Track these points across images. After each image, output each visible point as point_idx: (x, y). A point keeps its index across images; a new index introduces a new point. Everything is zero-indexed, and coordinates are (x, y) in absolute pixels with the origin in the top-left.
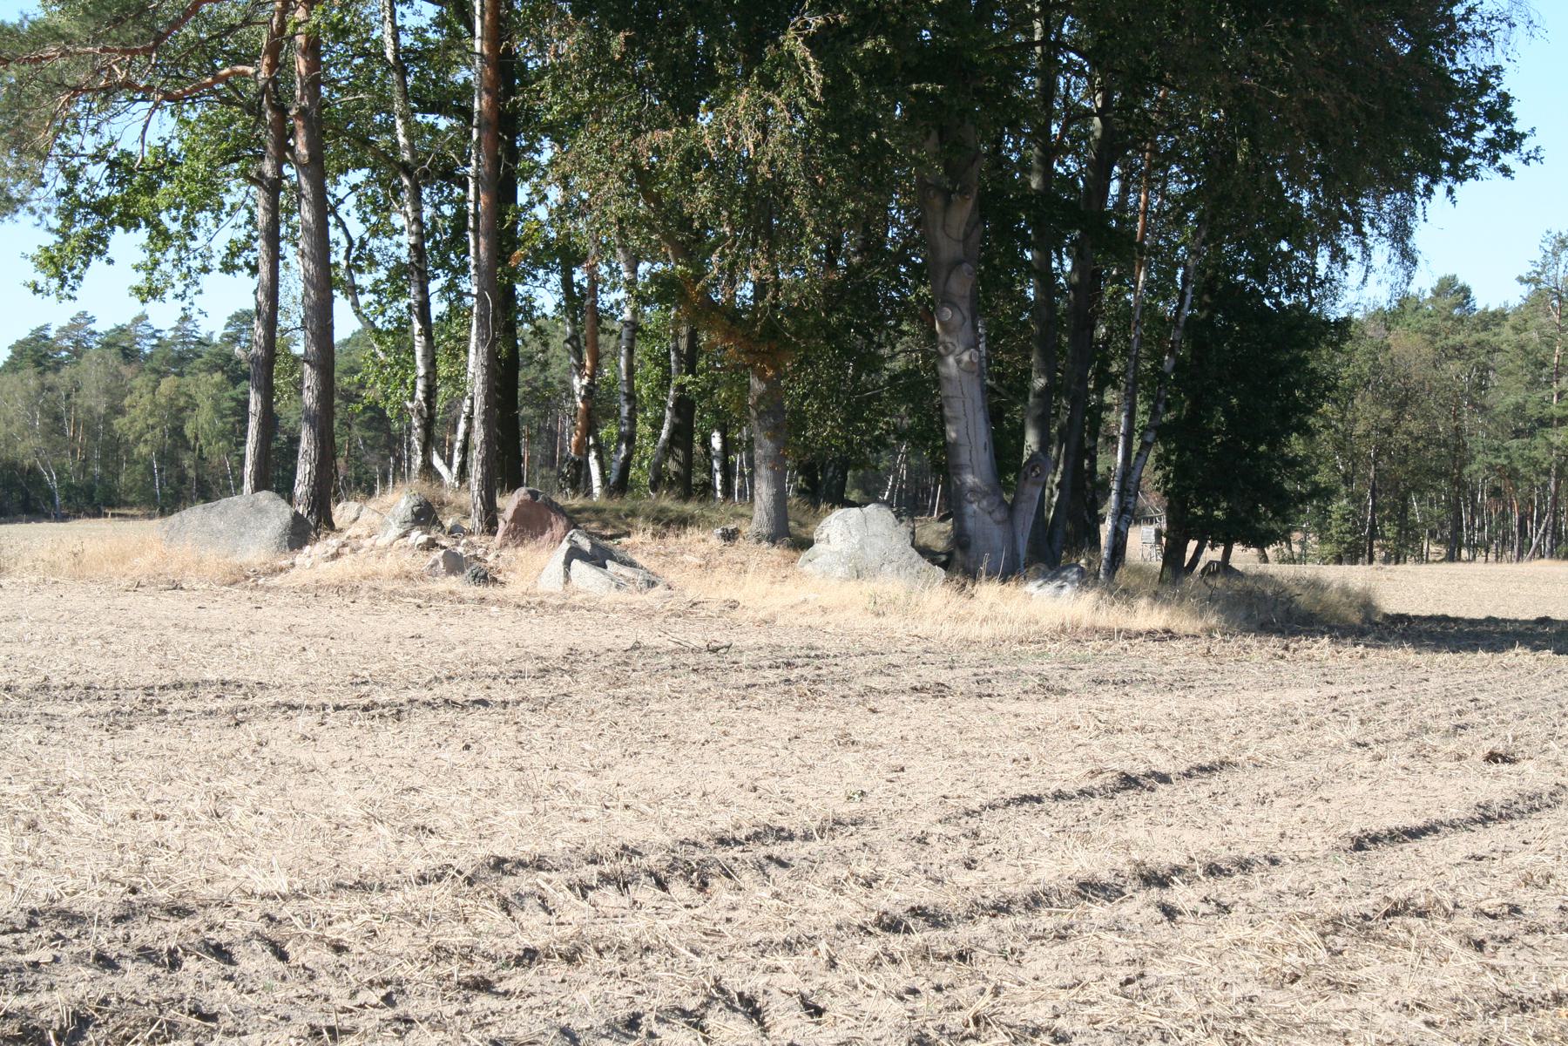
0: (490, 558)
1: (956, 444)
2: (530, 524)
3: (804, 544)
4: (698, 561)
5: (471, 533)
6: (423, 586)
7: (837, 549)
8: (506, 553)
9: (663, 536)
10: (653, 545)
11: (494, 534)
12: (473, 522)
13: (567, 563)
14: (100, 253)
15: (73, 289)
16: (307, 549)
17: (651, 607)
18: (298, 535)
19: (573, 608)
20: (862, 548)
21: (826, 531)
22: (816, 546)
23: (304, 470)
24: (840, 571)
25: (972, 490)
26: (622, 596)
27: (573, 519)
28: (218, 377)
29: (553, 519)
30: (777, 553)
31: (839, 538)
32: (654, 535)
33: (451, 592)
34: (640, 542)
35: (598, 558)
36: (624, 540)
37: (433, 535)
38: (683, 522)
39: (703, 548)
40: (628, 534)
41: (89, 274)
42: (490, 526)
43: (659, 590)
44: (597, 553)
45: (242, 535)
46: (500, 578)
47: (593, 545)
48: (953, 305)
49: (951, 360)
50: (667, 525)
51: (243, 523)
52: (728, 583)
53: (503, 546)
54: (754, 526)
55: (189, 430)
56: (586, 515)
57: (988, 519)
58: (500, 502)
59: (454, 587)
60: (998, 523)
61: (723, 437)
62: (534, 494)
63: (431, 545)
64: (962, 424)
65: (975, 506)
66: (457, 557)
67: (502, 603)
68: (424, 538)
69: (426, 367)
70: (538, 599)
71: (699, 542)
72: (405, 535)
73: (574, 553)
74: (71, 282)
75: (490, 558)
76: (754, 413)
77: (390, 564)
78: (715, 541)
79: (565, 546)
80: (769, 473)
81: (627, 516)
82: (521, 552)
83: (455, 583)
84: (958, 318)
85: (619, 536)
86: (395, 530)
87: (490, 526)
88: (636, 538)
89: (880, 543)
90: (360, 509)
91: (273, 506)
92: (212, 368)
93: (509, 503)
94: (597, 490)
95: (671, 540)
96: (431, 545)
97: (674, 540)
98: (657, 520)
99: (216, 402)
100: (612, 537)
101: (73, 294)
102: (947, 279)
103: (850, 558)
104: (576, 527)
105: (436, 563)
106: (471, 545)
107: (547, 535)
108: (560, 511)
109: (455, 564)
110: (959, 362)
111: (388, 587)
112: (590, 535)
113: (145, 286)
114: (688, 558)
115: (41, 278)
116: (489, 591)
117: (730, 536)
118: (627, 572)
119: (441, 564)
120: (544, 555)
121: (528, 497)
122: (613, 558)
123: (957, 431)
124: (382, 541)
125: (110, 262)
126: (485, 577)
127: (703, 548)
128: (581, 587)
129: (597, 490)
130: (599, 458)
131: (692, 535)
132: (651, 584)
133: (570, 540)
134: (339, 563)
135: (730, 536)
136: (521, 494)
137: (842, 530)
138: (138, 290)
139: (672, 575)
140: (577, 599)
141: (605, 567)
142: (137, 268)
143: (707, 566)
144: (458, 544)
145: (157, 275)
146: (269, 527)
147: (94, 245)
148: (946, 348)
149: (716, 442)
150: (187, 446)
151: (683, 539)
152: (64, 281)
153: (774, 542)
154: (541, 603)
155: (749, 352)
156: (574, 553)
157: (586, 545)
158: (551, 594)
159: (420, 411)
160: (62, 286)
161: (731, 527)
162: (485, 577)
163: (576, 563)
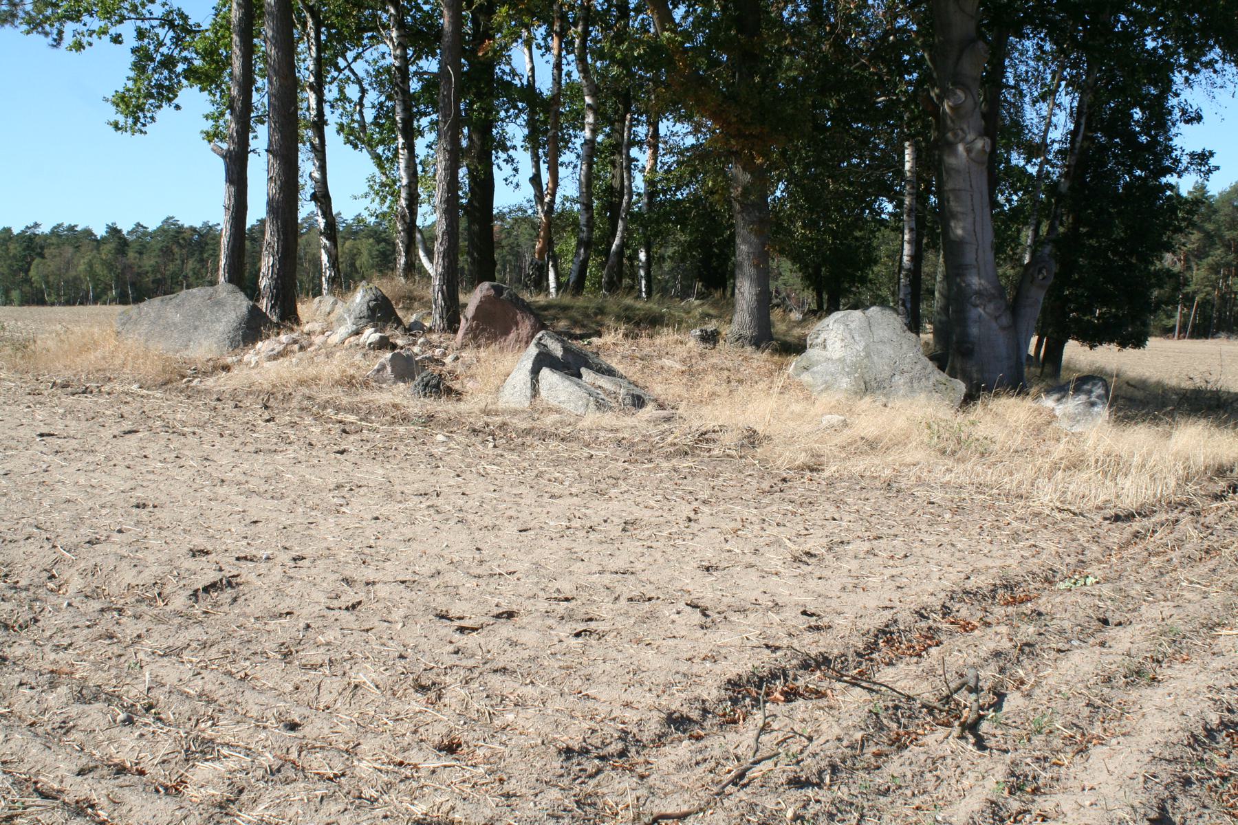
0: (448, 360)
1: (961, 243)
2: (494, 324)
3: (795, 348)
4: (678, 366)
5: (431, 330)
6: (367, 395)
7: (836, 356)
8: (467, 355)
9: (635, 337)
10: (626, 347)
11: (455, 332)
12: (434, 319)
13: (535, 372)
14: (170, 100)
15: (144, 125)
16: (260, 344)
17: (646, 438)
18: (252, 329)
19: (544, 436)
20: (868, 356)
21: (823, 336)
22: (810, 352)
23: (267, 263)
24: (845, 382)
25: (979, 293)
26: (608, 419)
27: (541, 319)
28: (371, 240)
29: (519, 317)
30: (761, 359)
31: (838, 344)
32: (626, 336)
33: (395, 406)
34: (611, 343)
35: (571, 366)
36: (595, 340)
37: (387, 334)
38: (654, 322)
39: (681, 351)
40: (599, 335)
41: (159, 115)
42: (452, 324)
43: (649, 411)
44: (570, 359)
45: (196, 328)
46: (457, 386)
47: (566, 350)
48: (966, 88)
49: (961, 148)
50: (638, 324)
51: (199, 315)
52: (695, 378)
53: (464, 346)
54: (735, 327)
55: (358, 264)
56: (552, 312)
57: (994, 324)
58: (462, 298)
59: (398, 400)
60: (1003, 328)
61: (648, 252)
62: (498, 290)
63: (384, 344)
64: (970, 220)
65: (981, 310)
66: (409, 359)
67: (449, 424)
68: (376, 336)
69: (409, 177)
70: (498, 420)
71: (674, 347)
72: (358, 333)
73: (544, 360)
74: (142, 120)
75: (448, 360)
76: (738, 207)
77: (332, 368)
78: (692, 342)
79: (533, 351)
80: (752, 271)
81: (596, 314)
82: (483, 354)
83: (401, 394)
84: (970, 102)
85: (589, 336)
86: (349, 326)
87: (452, 324)
88: (608, 339)
89: (889, 351)
90: (335, 303)
91: (230, 299)
92: (369, 237)
93: (472, 300)
94: (552, 290)
95: (644, 341)
96: (384, 344)
97: (647, 341)
98: (628, 320)
99: (370, 251)
100: (582, 337)
101: (144, 129)
102: (959, 58)
103: (855, 367)
104: (544, 327)
105: (383, 367)
106: (429, 345)
107: (512, 336)
108: (527, 308)
109: (405, 369)
110: (968, 151)
111: (323, 397)
112: (559, 335)
113: (211, 130)
114: (667, 362)
115: (121, 119)
116: (443, 407)
117: (710, 338)
118: (603, 381)
119: (389, 369)
120: (508, 359)
121: (492, 292)
122: (589, 366)
123: (964, 229)
124: (335, 339)
125: (178, 107)
126: (437, 386)
127: (681, 351)
128: (553, 403)
129: (552, 290)
130: (555, 267)
131: (666, 337)
132: (638, 402)
133: (538, 344)
134: (284, 362)
135: (710, 338)
136: (484, 289)
137: (839, 337)
138: (207, 133)
139: (658, 389)
140: (549, 420)
141: (579, 376)
142: (207, 117)
143: (691, 374)
144: (414, 343)
145: (221, 122)
146: (225, 320)
147: (166, 93)
148: (956, 135)
149: (642, 256)
150: (357, 272)
151: (658, 341)
152: (136, 120)
153: (758, 347)
154: (503, 426)
155: (739, 135)
156: (544, 360)
157: (557, 349)
158: (515, 413)
159: (403, 217)
160: (135, 123)
161: (710, 327)
162: (437, 386)
163: (545, 373)
